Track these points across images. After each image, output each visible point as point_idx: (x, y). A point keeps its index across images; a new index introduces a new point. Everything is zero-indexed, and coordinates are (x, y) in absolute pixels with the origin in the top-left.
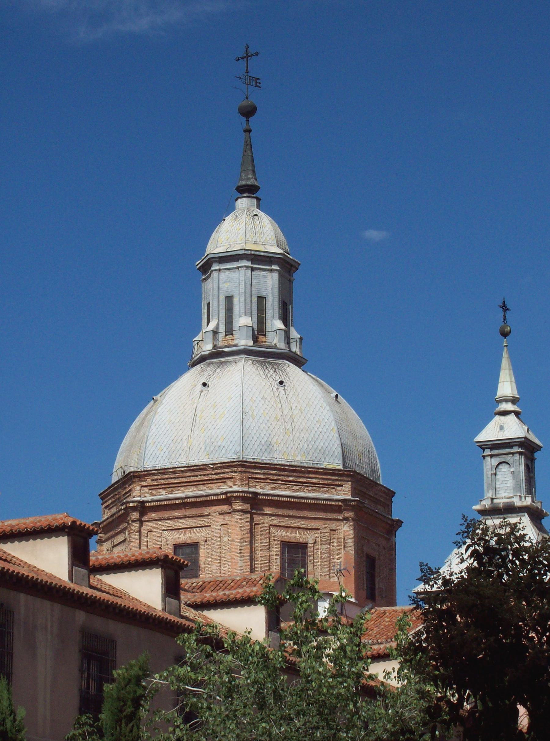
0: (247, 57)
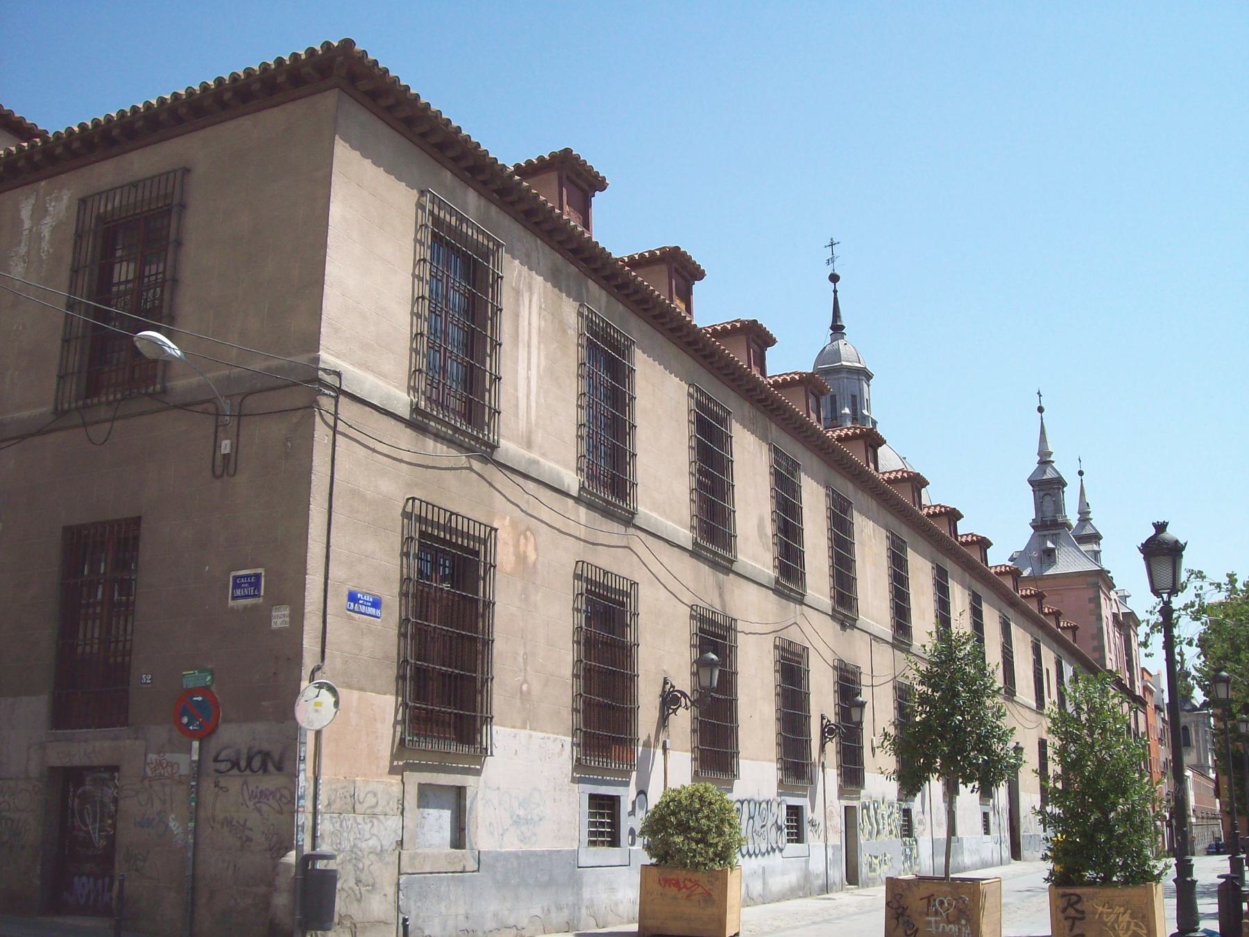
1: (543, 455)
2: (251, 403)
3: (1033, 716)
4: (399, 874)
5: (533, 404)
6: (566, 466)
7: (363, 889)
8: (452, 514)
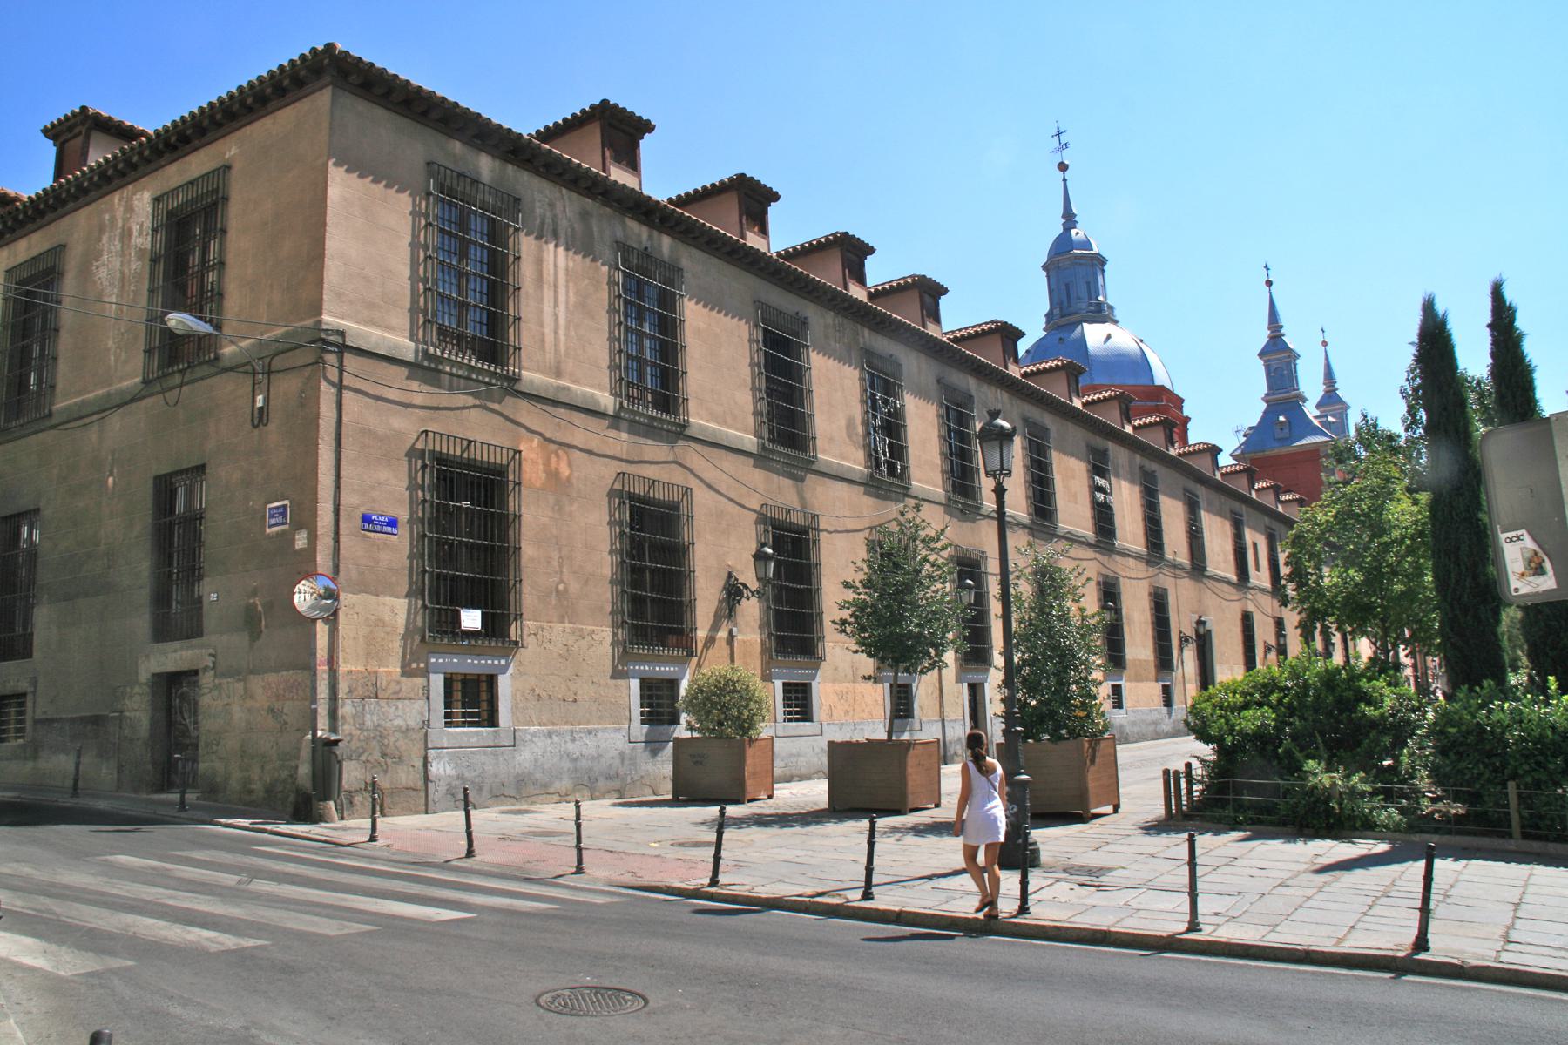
0: (1059, 134)
1: (574, 382)
2: (277, 363)
3: (1231, 592)
4: (427, 748)
5: (562, 338)
6: (601, 389)
7: (389, 761)
8: (470, 442)
